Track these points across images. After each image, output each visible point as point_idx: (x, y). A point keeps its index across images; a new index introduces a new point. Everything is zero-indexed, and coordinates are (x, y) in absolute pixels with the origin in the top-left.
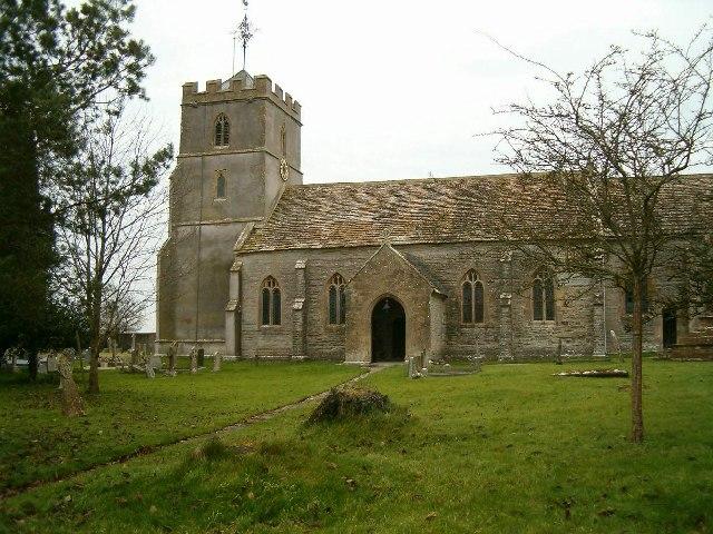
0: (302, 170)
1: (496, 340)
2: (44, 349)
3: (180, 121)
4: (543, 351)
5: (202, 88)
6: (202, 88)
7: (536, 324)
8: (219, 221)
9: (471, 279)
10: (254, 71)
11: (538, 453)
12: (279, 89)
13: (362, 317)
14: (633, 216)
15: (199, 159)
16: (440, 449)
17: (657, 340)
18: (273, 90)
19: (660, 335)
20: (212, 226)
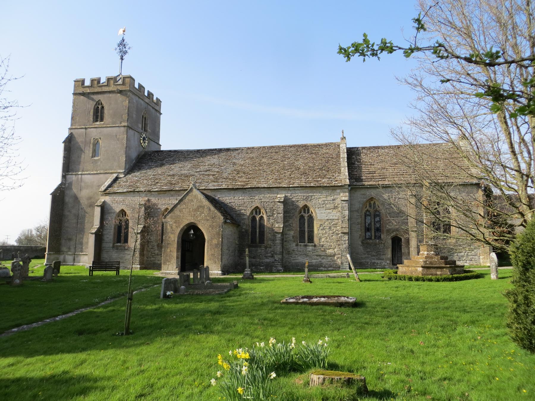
0: (160, 143)
1: (272, 256)
2: (141, 236)
3: (72, 104)
4: (313, 231)
5: (87, 83)
6: (87, 83)
7: (301, 247)
8: (95, 172)
9: (256, 213)
10: (125, 73)
11: (327, 153)
12: (150, 95)
13: (173, 238)
14: (479, 105)
15: (84, 130)
16: (455, 60)
17: (387, 259)
18: (146, 94)
19: (389, 255)
20: (89, 176)
